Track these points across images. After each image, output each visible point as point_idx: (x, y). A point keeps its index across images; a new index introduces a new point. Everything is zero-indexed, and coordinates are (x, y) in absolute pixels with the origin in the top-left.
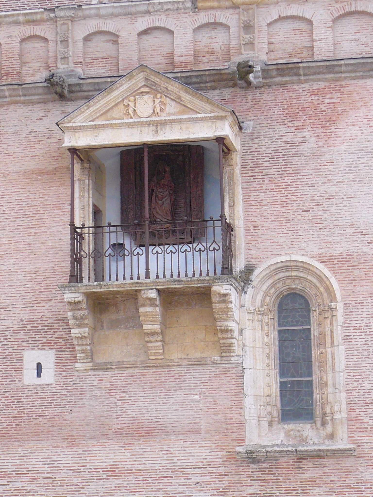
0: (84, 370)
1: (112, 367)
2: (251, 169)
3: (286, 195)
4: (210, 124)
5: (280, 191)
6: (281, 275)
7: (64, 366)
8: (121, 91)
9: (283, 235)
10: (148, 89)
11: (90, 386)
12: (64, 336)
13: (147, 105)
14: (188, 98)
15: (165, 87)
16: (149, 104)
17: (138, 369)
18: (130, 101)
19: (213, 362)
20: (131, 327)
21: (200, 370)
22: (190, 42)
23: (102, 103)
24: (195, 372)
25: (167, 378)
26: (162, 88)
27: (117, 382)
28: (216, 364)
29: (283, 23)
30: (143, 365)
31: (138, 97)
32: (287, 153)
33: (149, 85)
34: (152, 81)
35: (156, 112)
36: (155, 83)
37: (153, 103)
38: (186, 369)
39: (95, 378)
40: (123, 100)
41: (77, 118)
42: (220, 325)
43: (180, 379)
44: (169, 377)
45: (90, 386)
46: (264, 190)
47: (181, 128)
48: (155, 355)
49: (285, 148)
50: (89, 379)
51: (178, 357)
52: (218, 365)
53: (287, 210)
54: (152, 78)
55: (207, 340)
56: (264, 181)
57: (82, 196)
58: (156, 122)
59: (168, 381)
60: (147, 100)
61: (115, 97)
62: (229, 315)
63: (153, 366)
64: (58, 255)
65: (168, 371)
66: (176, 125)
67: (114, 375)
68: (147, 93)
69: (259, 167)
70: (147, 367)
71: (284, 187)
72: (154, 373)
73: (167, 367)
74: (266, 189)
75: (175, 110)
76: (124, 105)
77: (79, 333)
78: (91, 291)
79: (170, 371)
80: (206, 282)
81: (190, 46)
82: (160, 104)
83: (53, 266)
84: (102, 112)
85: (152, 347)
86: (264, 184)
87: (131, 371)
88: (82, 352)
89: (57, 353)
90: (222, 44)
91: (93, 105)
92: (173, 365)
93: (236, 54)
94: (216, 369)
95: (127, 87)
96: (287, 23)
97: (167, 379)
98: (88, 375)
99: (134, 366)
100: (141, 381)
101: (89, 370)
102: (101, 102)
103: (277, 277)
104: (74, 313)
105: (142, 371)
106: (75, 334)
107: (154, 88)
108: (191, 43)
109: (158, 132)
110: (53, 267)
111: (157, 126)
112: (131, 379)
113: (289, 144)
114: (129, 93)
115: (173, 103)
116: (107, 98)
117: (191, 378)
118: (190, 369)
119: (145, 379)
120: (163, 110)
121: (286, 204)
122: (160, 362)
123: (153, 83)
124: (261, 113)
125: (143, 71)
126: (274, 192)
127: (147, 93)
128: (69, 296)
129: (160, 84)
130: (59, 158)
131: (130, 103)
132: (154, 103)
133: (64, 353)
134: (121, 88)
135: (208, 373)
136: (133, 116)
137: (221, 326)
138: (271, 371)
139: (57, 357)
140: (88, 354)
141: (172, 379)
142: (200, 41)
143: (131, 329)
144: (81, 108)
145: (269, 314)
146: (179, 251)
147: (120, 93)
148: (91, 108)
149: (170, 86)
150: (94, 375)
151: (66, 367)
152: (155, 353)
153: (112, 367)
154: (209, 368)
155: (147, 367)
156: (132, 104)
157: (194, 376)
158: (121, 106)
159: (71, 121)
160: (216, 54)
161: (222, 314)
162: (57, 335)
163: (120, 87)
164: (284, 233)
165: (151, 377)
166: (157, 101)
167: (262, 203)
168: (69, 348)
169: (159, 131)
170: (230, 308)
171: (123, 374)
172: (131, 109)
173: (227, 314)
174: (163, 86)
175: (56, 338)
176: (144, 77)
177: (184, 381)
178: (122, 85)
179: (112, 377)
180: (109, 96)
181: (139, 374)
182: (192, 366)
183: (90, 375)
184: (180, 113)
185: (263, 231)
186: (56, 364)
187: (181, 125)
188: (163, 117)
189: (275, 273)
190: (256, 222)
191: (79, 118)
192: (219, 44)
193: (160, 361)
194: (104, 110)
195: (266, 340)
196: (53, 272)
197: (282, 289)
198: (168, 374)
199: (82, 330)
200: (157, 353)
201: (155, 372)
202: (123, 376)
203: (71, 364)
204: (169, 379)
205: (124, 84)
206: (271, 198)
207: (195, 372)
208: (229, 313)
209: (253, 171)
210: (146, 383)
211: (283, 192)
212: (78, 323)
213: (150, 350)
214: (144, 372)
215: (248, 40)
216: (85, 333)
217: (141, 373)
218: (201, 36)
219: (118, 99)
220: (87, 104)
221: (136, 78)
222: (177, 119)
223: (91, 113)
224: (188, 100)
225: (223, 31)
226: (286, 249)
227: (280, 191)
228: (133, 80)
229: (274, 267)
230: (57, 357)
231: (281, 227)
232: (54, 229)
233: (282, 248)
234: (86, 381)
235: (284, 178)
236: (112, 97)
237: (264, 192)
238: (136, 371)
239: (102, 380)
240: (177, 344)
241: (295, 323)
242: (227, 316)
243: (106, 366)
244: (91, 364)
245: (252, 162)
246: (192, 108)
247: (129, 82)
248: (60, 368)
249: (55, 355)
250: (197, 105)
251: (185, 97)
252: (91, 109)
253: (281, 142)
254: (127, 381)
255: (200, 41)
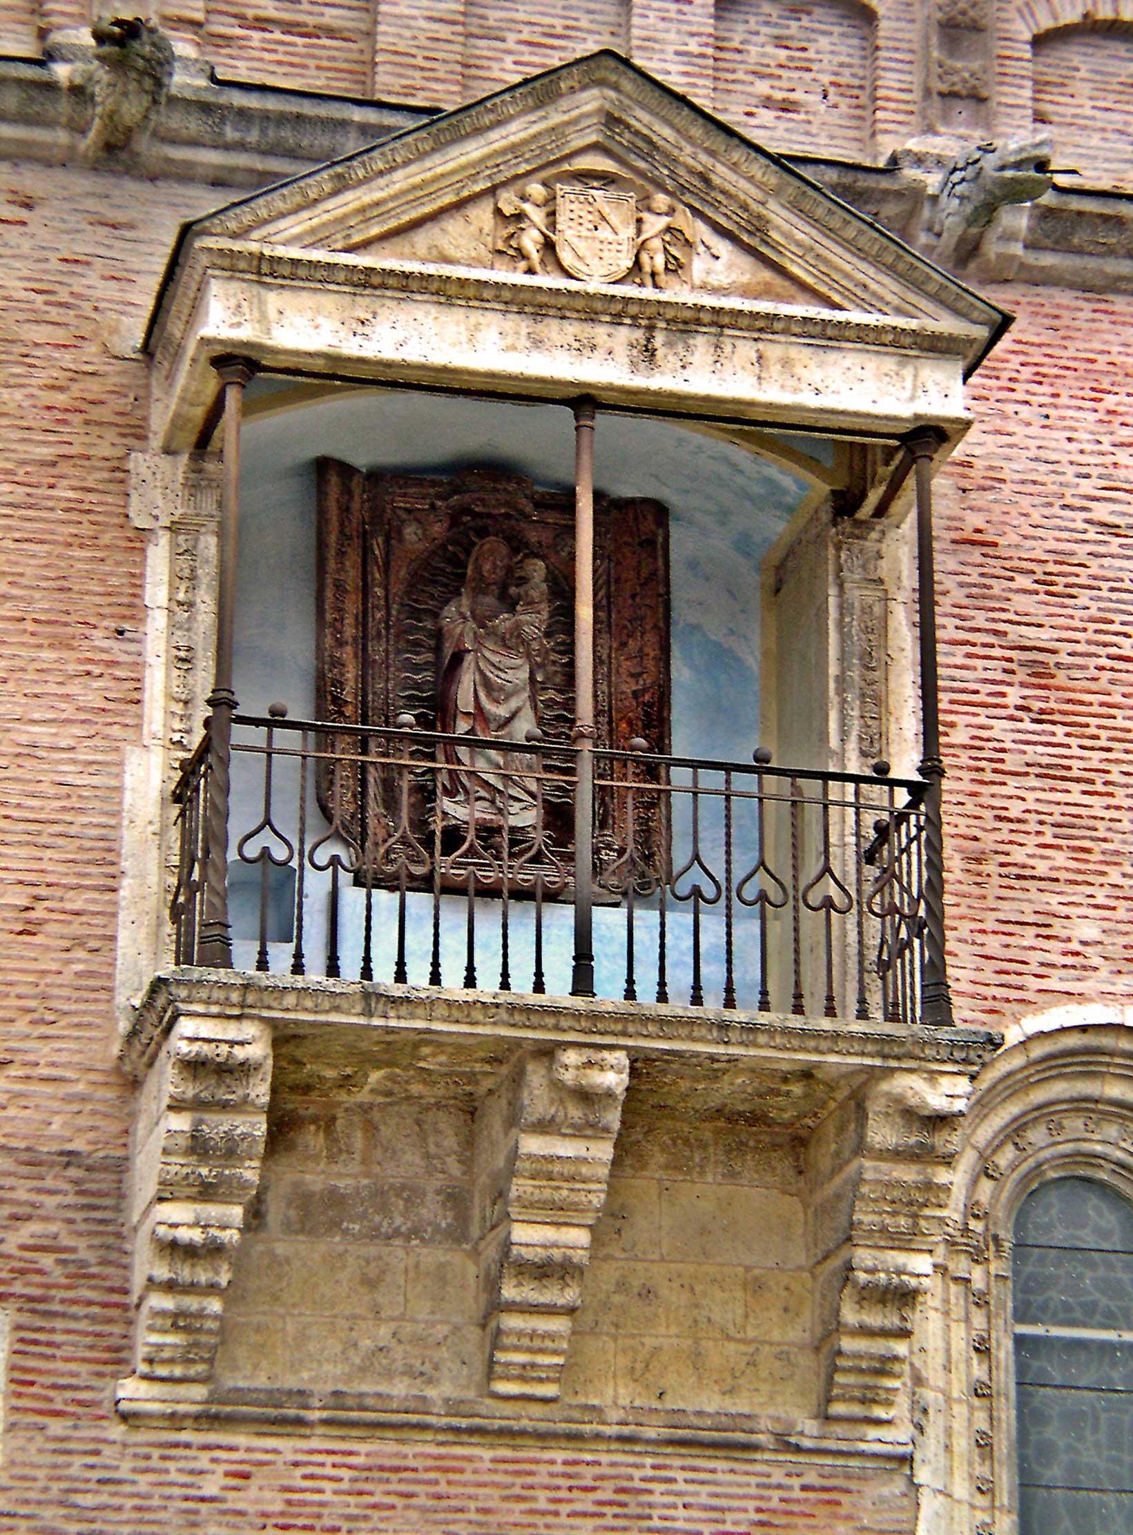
0: (163, 1416)
1: (302, 1413)
2: (956, 611)
3: (1103, 743)
4: (890, 364)
5: (1081, 725)
6: (1058, 1089)
7: (54, 1387)
8: (496, 146)
9: (1092, 912)
10: (611, 163)
11: (187, 1499)
12: (66, 1241)
13: (604, 233)
14: (800, 236)
15: (700, 168)
16: (619, 227)
17: (429, 1436)
18: (524, 198)
19: (785, 1444)
20: (397, 1233)
21: (713, 1471)
22: (704, 39)
23: (401, 180)
24: (693, 1481)
25: (563, 1494)
26: (681, 171)
27: (320, 1491)
28: (798, 1449)
29: (1090, 50)
30: (455, 1421)
31: (567, 188)
32: (1111, 574)
33: (617, 149)
34: (637, 133)
35: (647, 269)
36: (650, 142)
37: (631, 231)
38: (649, 1461)
39: (214, 1460)
40: (492, 191)
41: (282, 224)
42: (870, 1263)
43: (623, 1505)
44: (570, 1489)
45: (187, 1499)
46: (1011, 711)
47: (760, 357)
48: (525, 1373)
49: (1102, 549)
50: (181, 1464)
51: (616, 1397)
52: (801, 1458)
53: (1108, 808)
54: (641, 119)
55: (751, 1333)
56: (1013, 672)
57: (180, 604)
58: (650, 311)
59: (565, 1508)
60: (606, 210)
61: (463, 168)
62: (923, 1223)
63: (502, 1432)
64: (48, 853)
65: (566, 1463)
66: (739, 343)
67: (305, 1458)
68: (607, 180)
69: (993, 610)
70: (472, 1431)
71: (1095, 709)
72: (502, 1466)
73: (563, 1444)
74: (1018, 708)
75: (733, 277)
76: (498, 212)
77: (196, 1224)
78: (322, 1018)
79: (575, 1463)
80: (870, 1048)
81: (703, 56)
82: (667, 238)
83: (25, 902)
84: (393, 224)
85: (520, 1334)
86: (1010, 684)
87: (384, 1448)
88: (174, 1325)
89: (25, 1319)
90: (833, 78)
91: (361, 183)
92: (598, 1437)
93: (903, 129)
94: (789, 1475)
95: (523, 135)
96: (1107, 52)
97: (559, 1501)
98: (176, 1445)
99: (414, 1418)
100: (439, 1497)
101: (186, 1416)
102: (399, 175)
103: (1039, 1096)
104: (201, 1122)
105: (442, 1450)
106: (174, 1226)
107: (641, 165)
108: (707, 45)
109: (653, 355)
110: (27, 909)
111: (651, 328)
112: (388, 1481)
113: (1118, 535)
114: (524, 168)
115: (722, 247)
116: (428, 163)
117: (675, 1506)
118: (668, 1461)
119: (453, 1490)
120: (681, 266)
121: (1106, 783)
122: (538, 1415)
123: (640, 144)
124: (1001, 389)
125: (601, 83)
126: (1054, 723)
127: (607, 180)
128: (207, 1029)
129: (676, 152)
130: (76, 418)
131: (528, 207)
132: (639, 232)
133: (59, 1324)
134: (494, 135)
135: (753, 1491)
136: (538, 268)
137: (871, 1271)
138: (997, 1513)
139: (22, 1340)
140: (203, 1338)
141: (585, 1503)
142: (739, 51)
143: (398, 1242)
144: (310, 181)
145: (990, 1254)
146: (734, 894)
147: (489, 157)
148: (349, 196)
149: (720, 168)
150: (206, 1447)
151: (69, 1395)
152: (524, 1366)
153: (302, 1413)
154: (758, 1468)
155: (472, 1431)
156: (537, 215)
157: (687, 1500)
158: (482, 215)
159: (250, 229)
160: (802, 116)
161: (894, 1214)
162: (27, 1232)
163: (490, 128)
164: (1097, 907)
165: (483, 1485)
166: (654, 224)
167: (1002, 761)
168: (90, 1303)
169: (659, 354)
170: (939, 1186)
171: (350, 1453)
172: (535, 234)
173: (915, 1216)
174: (691, 162)
175: (24, 1247)
176: (600, 111)
177: (640, 1517)
178: (499, 123)
179: (296, 1464)
180: (437, 158)
181: (430, 1463)
182: (683, 1451)
183: (188, 1446)
184: (764, 292)
185: (1005, 882)
186: (18, 1375)
187: (760, 345)
188: (677, 293)
189: (1036, 1078)
190: (976, 839)
191: (294, 226)
192: (819, 76)
193: (536, 1410)
194: (405, 218)
195: (979, 1371)
196: (20, 933)
197: (1047, 1153)
198: (569, 1476)
199: (213, 1211)
200: (533, 1366)
201: (504, 1461)
202: (350, 1467)
203: (94, 1382)
204: (570, 1501)
205: (511, 118)
206: (1040, 749)
207: (693, 1481)
208: (927, 1212)
209: (968, 624)
210: (461, 1510)
211: (1092, 731)
212: (204, 1171)
213: (505, 1349)
214: (455, 1458)
215: (965, 81)
216: (224, 1227)
217: (441, 1457)
218: (741, 27)
219: (473, 178)
220: (339, 169)
221: (564, 104)
222: (755, 315)
223: (345, 217)
224: (799, 244)
225: (837, 29)
226: (1104, 973)
227: (1081, 725)
228: (550, 109)
229: (1047, 1047)
230: (22, 1340)
231: (1080, 878)
232: (41, 733)
233: (1084, 968)
234: (167, 1471)
235: (1096, 673)
236: (450, 166)
237: (1011, 718)
238: (419, 1450)
239: (246, 1476)
240: (615, 1339)
241: (1078, 1314)
242: (916, 1224)
243: (275, 1406)
244: (199, 1392)
245: (962, 585)
246: (810, 280)
247: (532, 118)
248: (34, 1396)
249: (19, 1327)
250: (837, 269)
251: (786, 227)
252: (352, 199)
253: (1087, 521)
254: (371, 1493)
255: (739, 51)
